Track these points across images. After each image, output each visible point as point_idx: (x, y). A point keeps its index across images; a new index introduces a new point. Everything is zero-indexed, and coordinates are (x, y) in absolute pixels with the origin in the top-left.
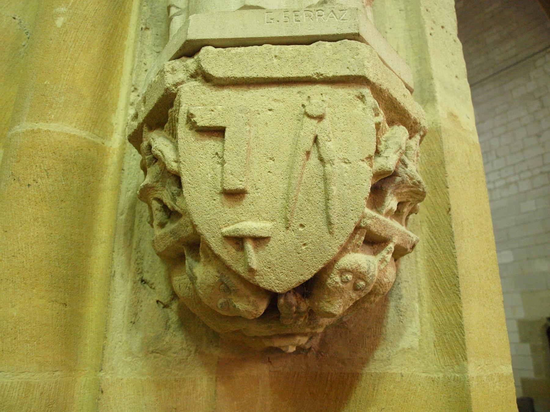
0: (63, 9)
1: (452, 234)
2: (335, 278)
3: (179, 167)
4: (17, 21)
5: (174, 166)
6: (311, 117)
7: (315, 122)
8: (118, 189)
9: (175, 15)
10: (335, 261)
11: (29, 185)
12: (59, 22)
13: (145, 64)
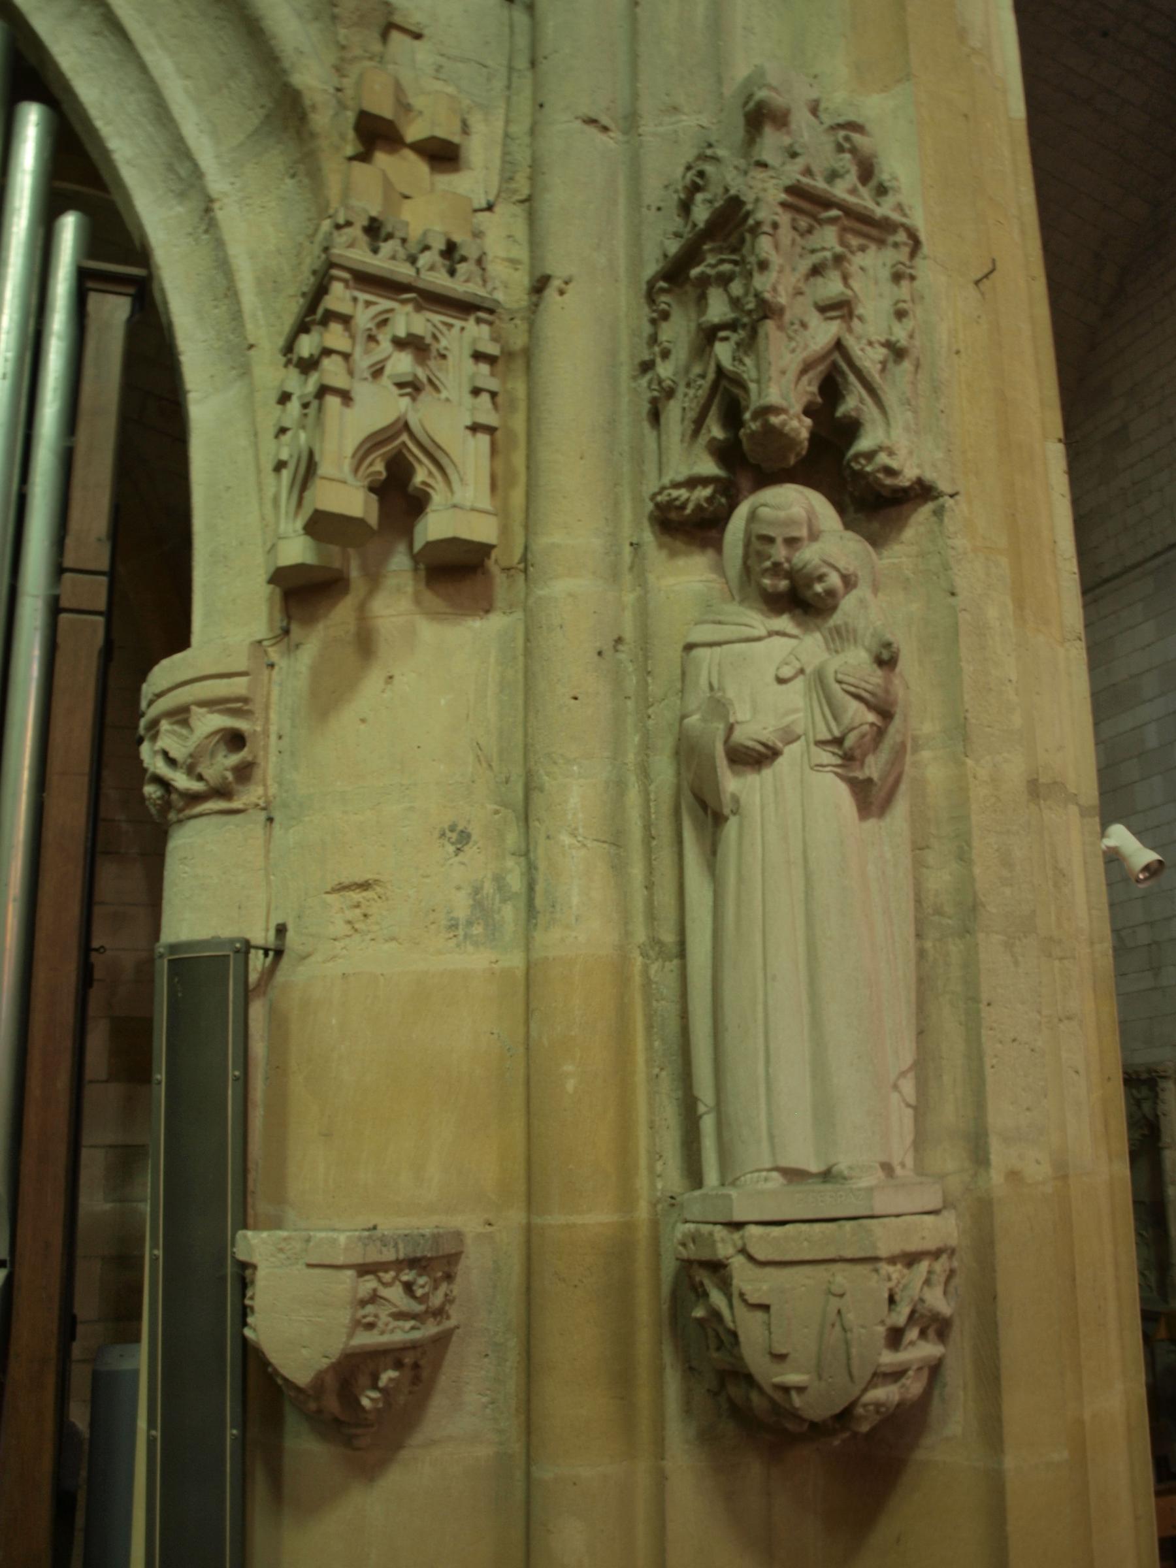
0: (569, 1068)
1: (996, 1324)
2: (860, 1410)
3: (736, 1326)
4: (496, 1036)
5: (731, 1325)
6: (835, 1295)
7: (837, 1299)
8: (656, 1269)
9: (706, 1113)
10: (858, 1398)
11: (576, 1286)
12: (570, 1086)
13: (666, 1119)
